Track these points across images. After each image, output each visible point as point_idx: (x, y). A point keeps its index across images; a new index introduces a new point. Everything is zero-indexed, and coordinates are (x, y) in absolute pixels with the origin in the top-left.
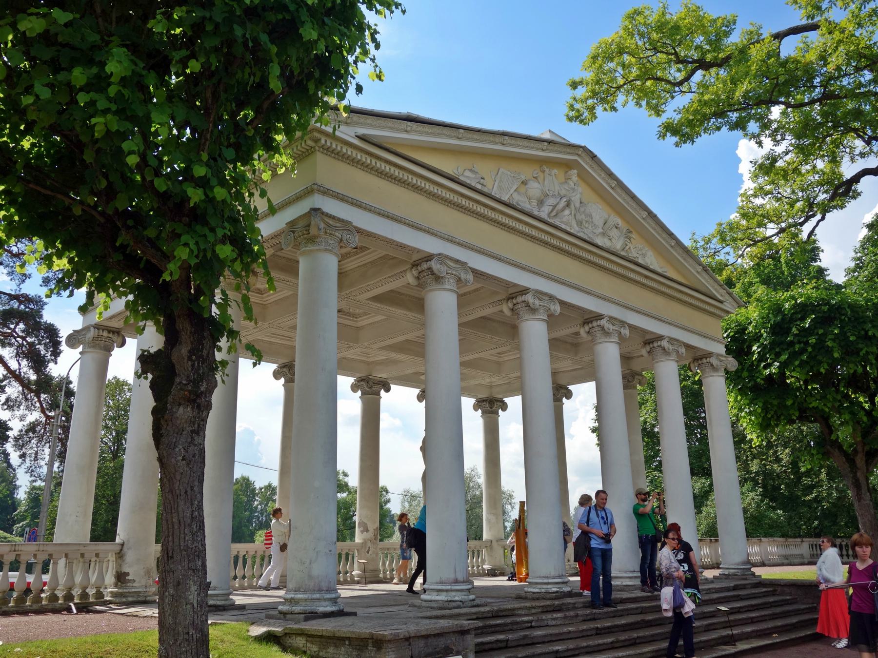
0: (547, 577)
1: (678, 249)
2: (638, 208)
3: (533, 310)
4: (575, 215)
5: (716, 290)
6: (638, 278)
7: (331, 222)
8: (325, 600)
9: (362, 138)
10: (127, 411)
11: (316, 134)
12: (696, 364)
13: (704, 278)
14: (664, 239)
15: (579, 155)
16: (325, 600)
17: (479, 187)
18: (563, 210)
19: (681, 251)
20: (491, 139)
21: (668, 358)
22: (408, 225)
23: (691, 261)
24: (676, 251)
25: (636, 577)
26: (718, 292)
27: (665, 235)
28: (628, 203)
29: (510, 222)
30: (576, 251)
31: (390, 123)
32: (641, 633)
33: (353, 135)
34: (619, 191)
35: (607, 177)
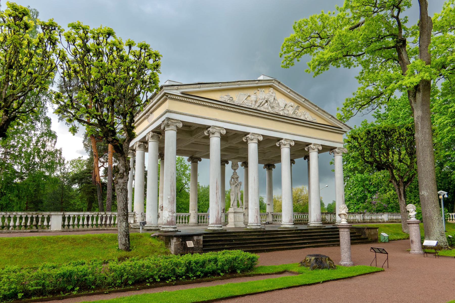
0: (252, 224)
1: (320, 111)
2: (300, 98)
3: (285, 145)
4: (270, 105)
5: (339, 124)
6: (309, 126)
7: (173, 121)
8: (171, 228)
9: (182, 93)
10: (344, 180)
11: (167, 95)
12: (331, 152)
13: (333, 120)
14: (313, 108)
15: (273, 83)
16: (171, 228)
17: (232, 103)
18: (264, 104)
19: (321, 111)
20: (234, 84)
21: (314, 151)
22: (257, 128)
23: (326, 114)
24: (319, 111)
25: (331, 220)
26: (340, 125)
27: (313, 106)
28: (296, 97)
29: (309, 126)
30: (311, 126)
31: (192, 86)
32: (329, 236)
33: (179, 93)
34: (292, 93)
35: (286, 89)
